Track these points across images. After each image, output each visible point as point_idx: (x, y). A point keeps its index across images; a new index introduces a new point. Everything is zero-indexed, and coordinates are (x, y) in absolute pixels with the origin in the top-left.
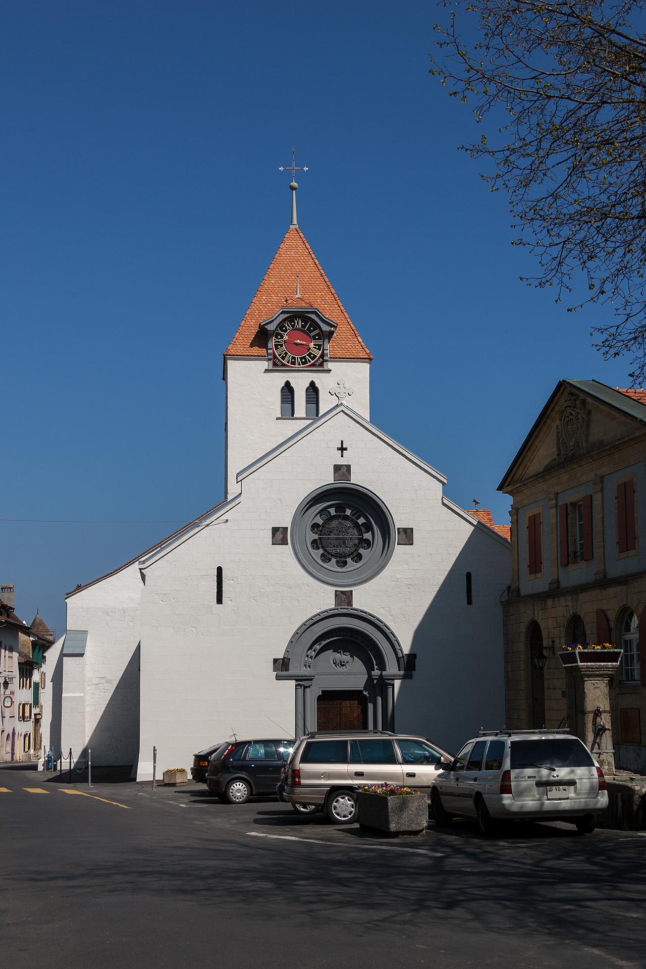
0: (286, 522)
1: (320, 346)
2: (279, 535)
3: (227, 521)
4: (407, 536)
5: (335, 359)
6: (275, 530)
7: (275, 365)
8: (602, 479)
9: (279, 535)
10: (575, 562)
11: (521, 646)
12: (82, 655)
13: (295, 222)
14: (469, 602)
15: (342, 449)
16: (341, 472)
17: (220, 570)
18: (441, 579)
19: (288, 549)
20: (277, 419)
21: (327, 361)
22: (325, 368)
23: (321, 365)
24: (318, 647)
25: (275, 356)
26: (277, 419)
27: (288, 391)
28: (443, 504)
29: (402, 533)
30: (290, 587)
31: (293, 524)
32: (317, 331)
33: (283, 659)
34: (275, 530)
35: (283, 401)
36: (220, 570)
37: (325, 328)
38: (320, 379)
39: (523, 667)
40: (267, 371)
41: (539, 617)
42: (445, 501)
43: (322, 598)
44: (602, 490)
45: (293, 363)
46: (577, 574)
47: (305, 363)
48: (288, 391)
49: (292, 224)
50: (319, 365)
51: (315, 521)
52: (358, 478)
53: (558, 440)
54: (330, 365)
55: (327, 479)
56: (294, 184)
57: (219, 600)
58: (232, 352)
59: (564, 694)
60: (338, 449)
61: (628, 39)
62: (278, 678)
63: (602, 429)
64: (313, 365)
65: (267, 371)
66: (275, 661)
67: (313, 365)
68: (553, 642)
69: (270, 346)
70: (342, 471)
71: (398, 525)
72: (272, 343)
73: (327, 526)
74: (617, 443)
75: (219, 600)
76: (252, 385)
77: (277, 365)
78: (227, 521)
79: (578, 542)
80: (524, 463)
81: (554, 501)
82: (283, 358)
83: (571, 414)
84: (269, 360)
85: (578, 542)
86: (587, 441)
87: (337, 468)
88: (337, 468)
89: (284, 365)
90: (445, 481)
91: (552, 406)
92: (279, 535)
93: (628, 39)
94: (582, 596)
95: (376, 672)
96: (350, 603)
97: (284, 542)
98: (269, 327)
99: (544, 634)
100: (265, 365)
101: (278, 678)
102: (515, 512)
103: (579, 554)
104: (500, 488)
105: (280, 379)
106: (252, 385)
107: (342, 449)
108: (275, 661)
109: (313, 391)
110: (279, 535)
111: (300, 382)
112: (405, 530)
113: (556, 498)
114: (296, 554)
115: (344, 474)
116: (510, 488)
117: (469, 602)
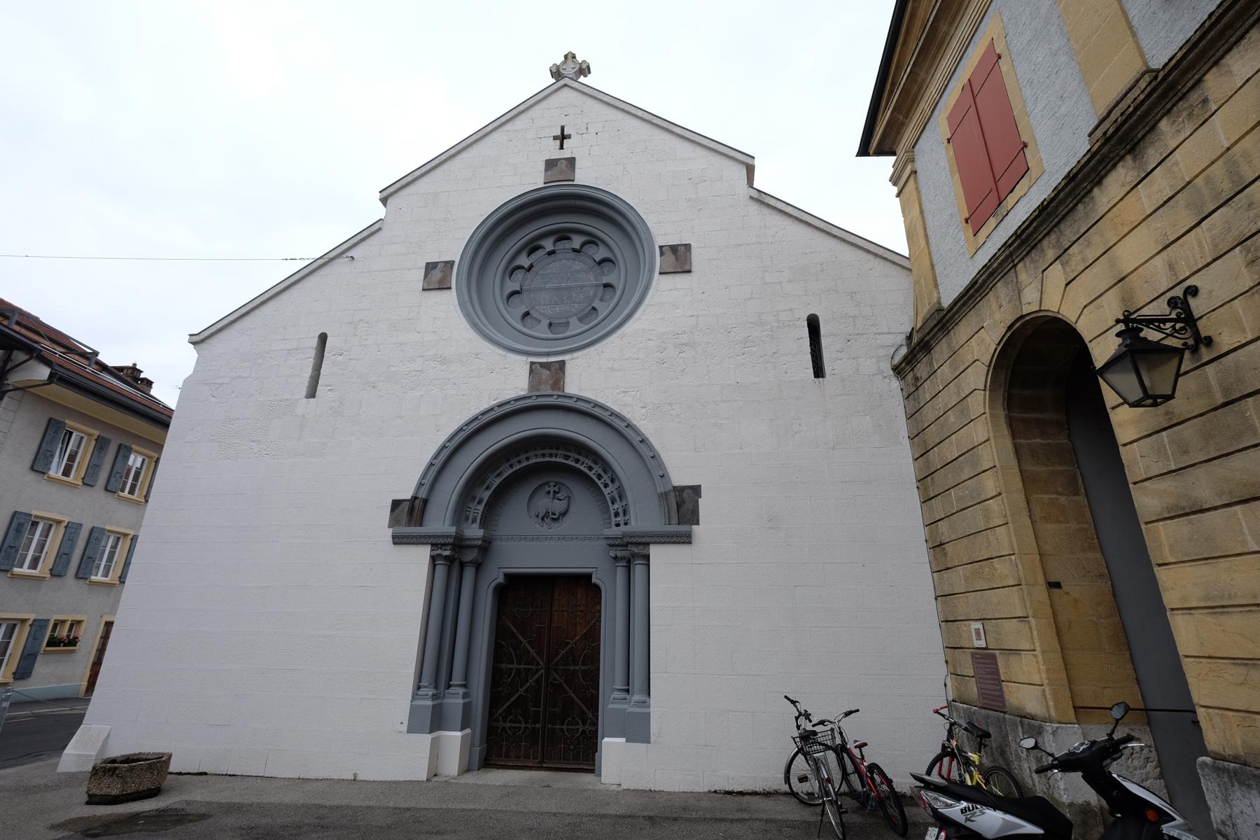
2: (437, 275)
4: (679, 258)
9: (437, 275)
11: (981, 432)
16: (556, 170)
24: (474, 276)
33: (415, 498)
34: (430, 267)
43: (508, 378)
51: (508, 290)
61: (928, 243)
62: (398, 540)
66: (396, 504)
71: (660, 241)
87: (551, 164)
93: (928, 243)
97: (443, 286)
101: (398, 540)
104: (864, 151)
108: (396, 504)
110: (436, 276)
112: (674, 249)
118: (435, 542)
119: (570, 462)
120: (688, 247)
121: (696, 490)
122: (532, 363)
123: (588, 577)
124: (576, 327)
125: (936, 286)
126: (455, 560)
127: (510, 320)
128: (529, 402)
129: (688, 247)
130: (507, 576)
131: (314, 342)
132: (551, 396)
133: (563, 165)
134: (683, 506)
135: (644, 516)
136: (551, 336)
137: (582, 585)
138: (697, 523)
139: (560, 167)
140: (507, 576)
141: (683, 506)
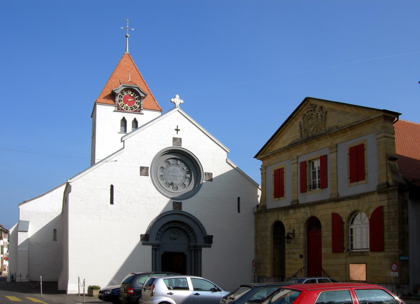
0: (148, 164)
1: (139, 103)
3: (116, 161)
5: (145, 109)
6: (142, 168)
7: (118, 109)
8: (337, 146)
9: (144, 171)
10: (310, 190)
11: (269, 233)
12: (27, 231)
13: (127, 51)
14: (239, 211)
15: (177, 130)
16: (177, 141)
17: (112, 187)
18: (24, 240)
19: (148, 179)
20: (119, 133)
21: (142, 110)
22: (141, 113)
23: (139, 111)
25: (118, 105)
26: (119, 133)
27: (124, 121)
28: (227, 162)
29: (207, 175)
30: (149, 198)
31: (151, 166)
32: (137, 97)
34: (142, 168)
35: (121, 126)
36: (112, 187)
37: (142, 95)
38: (138, 117)
39: (269, 243)
40: (114, 111)
41: (283, 218)
42: (228, 161)
44: (337, 151)
45: (127, 109)
46: (325, 194)
47: (132, 109)
48: (124, 121)
49: (126, 51)
50: (138, 111)
52: (186, 146)
53: (301, 129)
54: (143, 112)
55: (169, 144)
56: (128, 35)
57: (112, 202)
58: (99, 101)
59: (301, 256)
60: (176, 130)
63: (333, 121)
64: (136, 111)
65: (114, 111)
67: (136, 111)
68: (294, 231)
69: (116, 100)
70: (177, 141)
72: (117, 99)
73: (167, 169)
74: (354, 124)
75: (112, 202)
76: (108, 118)
77: (119, 109)
78: (116, 161)
79: (312, 181)
80: (273, 143)
81: (296, 160)
82: (122, 107)
83: (312, 114)
84: (116, 106)
85: (312, 181)
86: (325, 127)
87: (175, 139)
88: (175, 139)
89: (122, 109)
90: (229, 151)
91: (298, 111)
92: (144, 171)
94: (318, 207)
95: (192, 244)
96: (180, 208)
97: (146, 175)
98: (117, 92)
99: (286, 227)
100: (113, 108)
102: (264, 169)
103: (312, 186)
105: (120, 115)
106: (108, 118)
107: (177, 130)
109: (135, 122)
110: (144, 171)
111: (130, 118)
113: (297, 159)
114: (153, 181)
115: (178, 143)
116: (262, 156)
117: (239, 211)
118: (153, 245)
119: (175, 225)
120: (181, 139)
121: (212, 236)
122: (173, 202)
123: (184, 253)
124: (160, 173)
125: (266, 201)
126: (155, 249)
127: (170, 191)
128: (173, 212)
129: (181, 139)
130: (164, 252)
131: (110, 188)
132: (179, 211)
133: (179, 140)
134: (209, 240)
135: (200, 241)
136: (173, 191)
137: (182, 255)
138: (212, 243)
139: (177, 141)
140: (164, 252)
141: (209, 240)
